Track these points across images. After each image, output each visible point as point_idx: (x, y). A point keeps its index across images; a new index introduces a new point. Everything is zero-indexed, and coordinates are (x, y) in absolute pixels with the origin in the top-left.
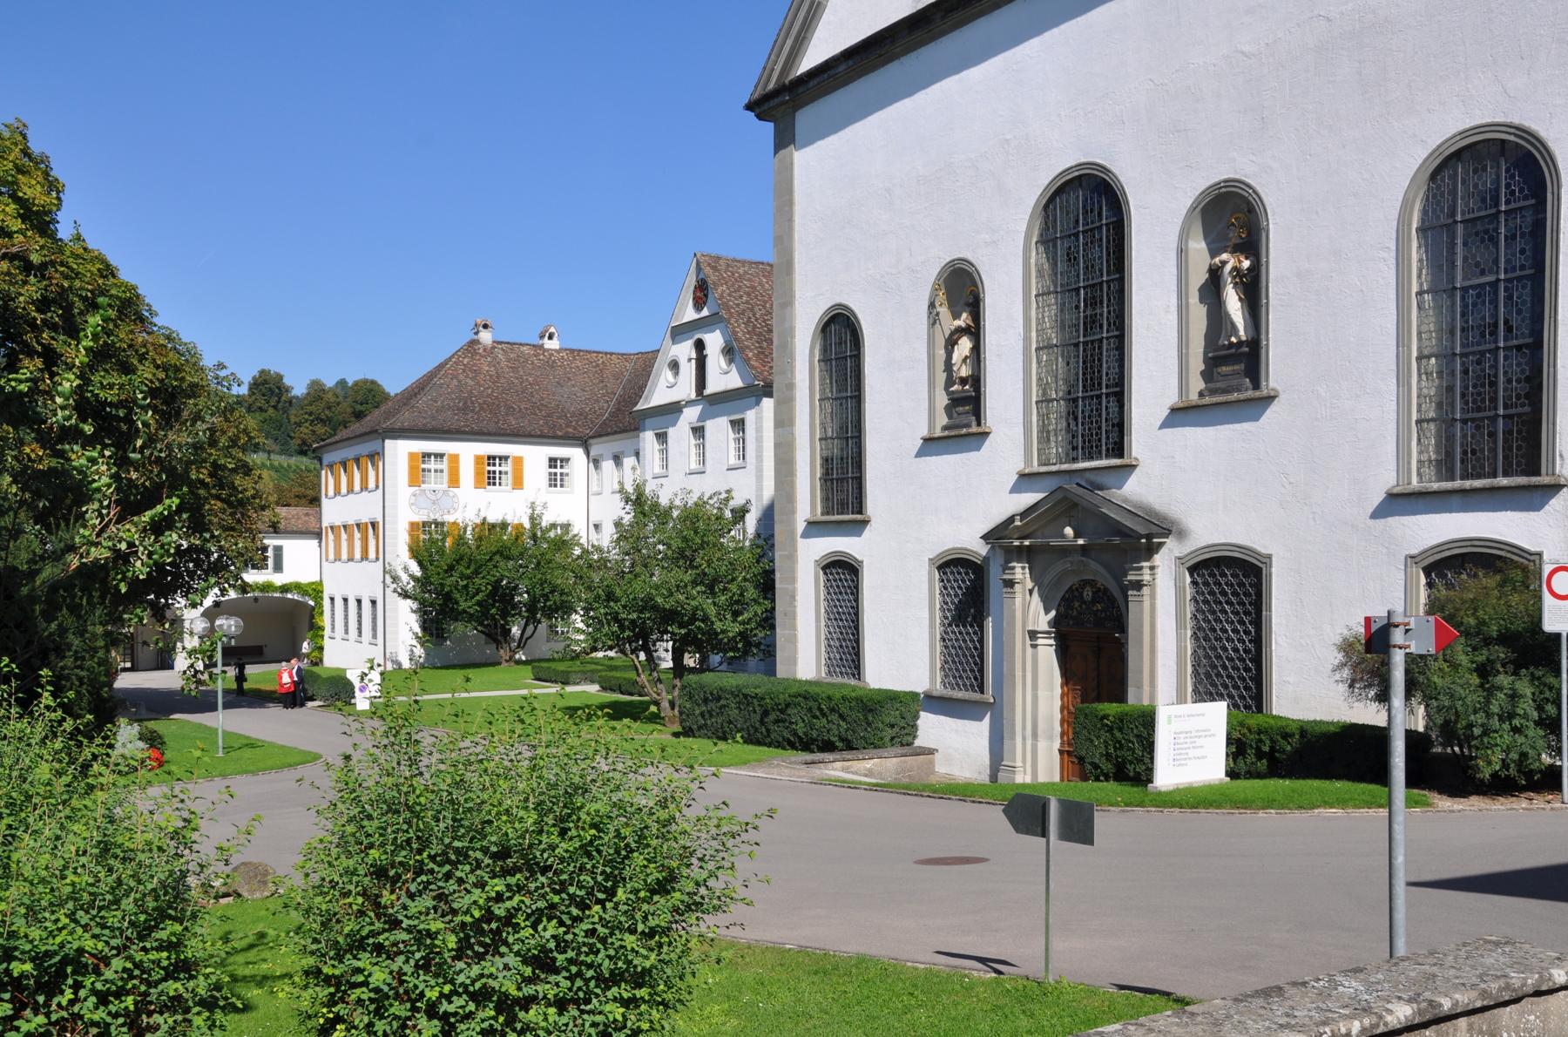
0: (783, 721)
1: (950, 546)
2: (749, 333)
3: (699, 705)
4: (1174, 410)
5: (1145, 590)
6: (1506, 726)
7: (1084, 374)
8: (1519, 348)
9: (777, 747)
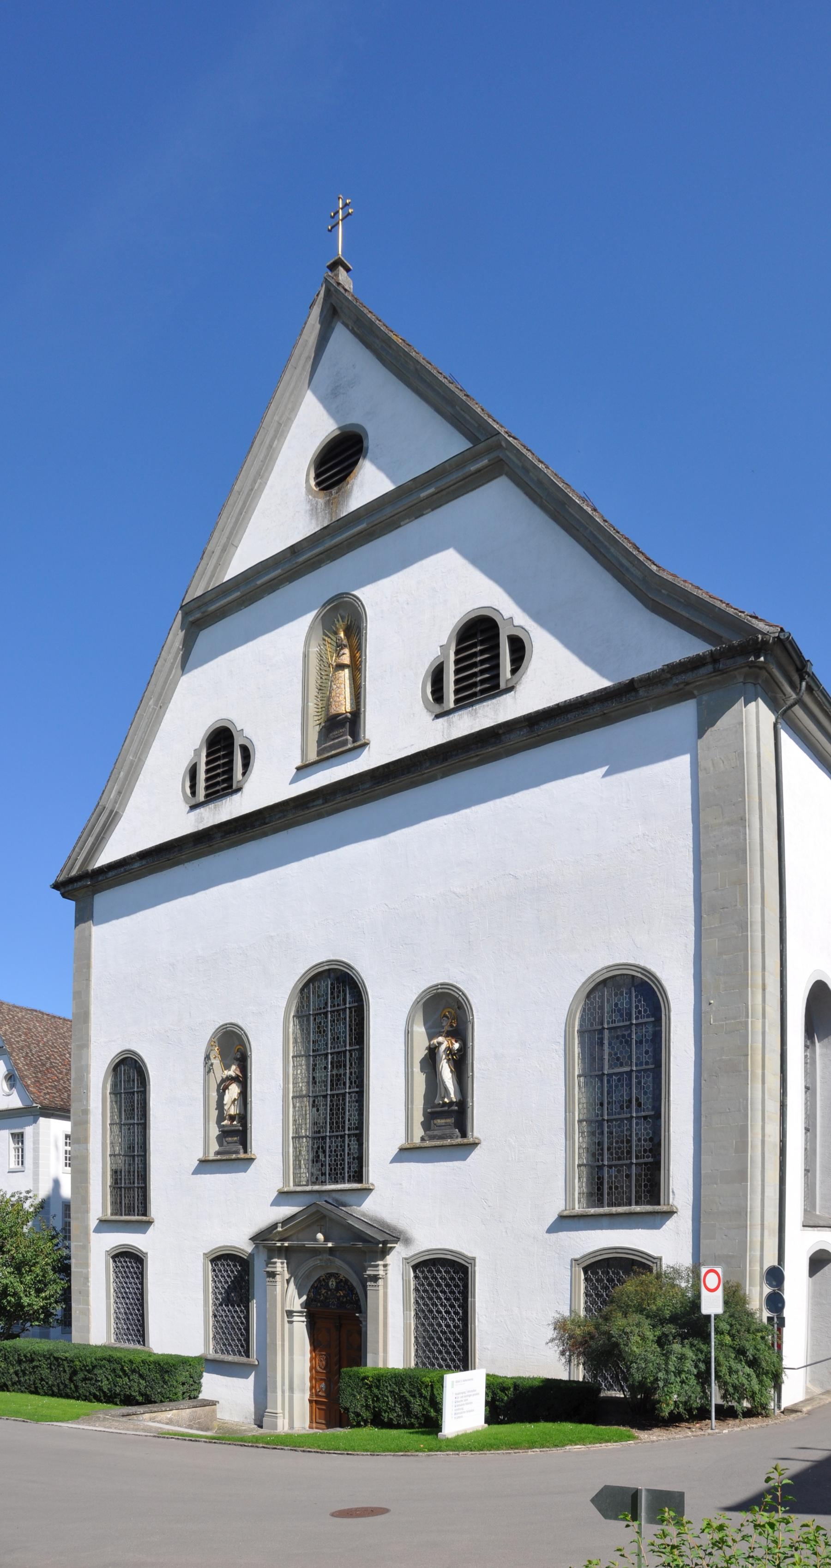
0: (90, 1379)
1: (222, 1244)
2: (27, 1065)
3: (13, 1365)
4: (402, 1150)
5: (380, 1282)
7: (331, 1119)
8: (645, 1118)
9: (85, 1400)
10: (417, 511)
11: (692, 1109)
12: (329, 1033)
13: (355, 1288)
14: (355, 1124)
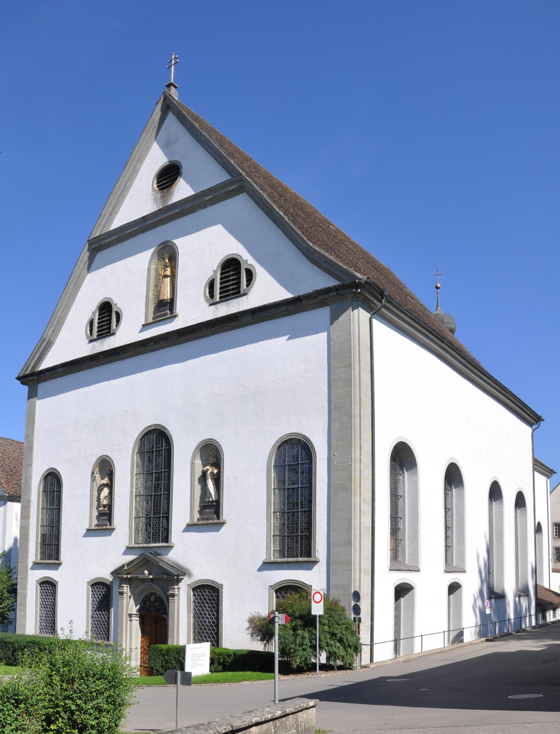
4: (188, 525)
5: (176, 598)
6: (301, 648)
7: (154, 508)
8: (305, 511)
10: (204, 205)
11: (326, 508)
12: (154, 462)
13: (164, 601)
14: (165, 511)
